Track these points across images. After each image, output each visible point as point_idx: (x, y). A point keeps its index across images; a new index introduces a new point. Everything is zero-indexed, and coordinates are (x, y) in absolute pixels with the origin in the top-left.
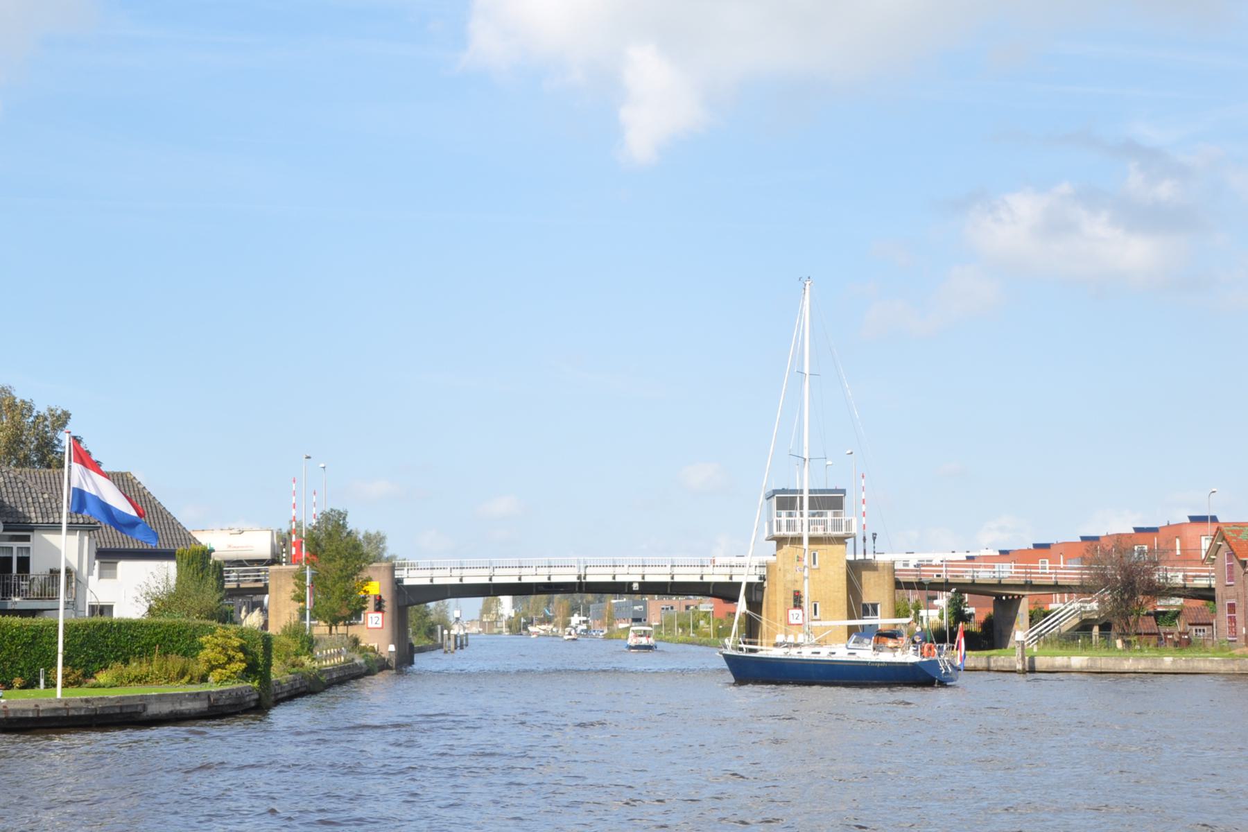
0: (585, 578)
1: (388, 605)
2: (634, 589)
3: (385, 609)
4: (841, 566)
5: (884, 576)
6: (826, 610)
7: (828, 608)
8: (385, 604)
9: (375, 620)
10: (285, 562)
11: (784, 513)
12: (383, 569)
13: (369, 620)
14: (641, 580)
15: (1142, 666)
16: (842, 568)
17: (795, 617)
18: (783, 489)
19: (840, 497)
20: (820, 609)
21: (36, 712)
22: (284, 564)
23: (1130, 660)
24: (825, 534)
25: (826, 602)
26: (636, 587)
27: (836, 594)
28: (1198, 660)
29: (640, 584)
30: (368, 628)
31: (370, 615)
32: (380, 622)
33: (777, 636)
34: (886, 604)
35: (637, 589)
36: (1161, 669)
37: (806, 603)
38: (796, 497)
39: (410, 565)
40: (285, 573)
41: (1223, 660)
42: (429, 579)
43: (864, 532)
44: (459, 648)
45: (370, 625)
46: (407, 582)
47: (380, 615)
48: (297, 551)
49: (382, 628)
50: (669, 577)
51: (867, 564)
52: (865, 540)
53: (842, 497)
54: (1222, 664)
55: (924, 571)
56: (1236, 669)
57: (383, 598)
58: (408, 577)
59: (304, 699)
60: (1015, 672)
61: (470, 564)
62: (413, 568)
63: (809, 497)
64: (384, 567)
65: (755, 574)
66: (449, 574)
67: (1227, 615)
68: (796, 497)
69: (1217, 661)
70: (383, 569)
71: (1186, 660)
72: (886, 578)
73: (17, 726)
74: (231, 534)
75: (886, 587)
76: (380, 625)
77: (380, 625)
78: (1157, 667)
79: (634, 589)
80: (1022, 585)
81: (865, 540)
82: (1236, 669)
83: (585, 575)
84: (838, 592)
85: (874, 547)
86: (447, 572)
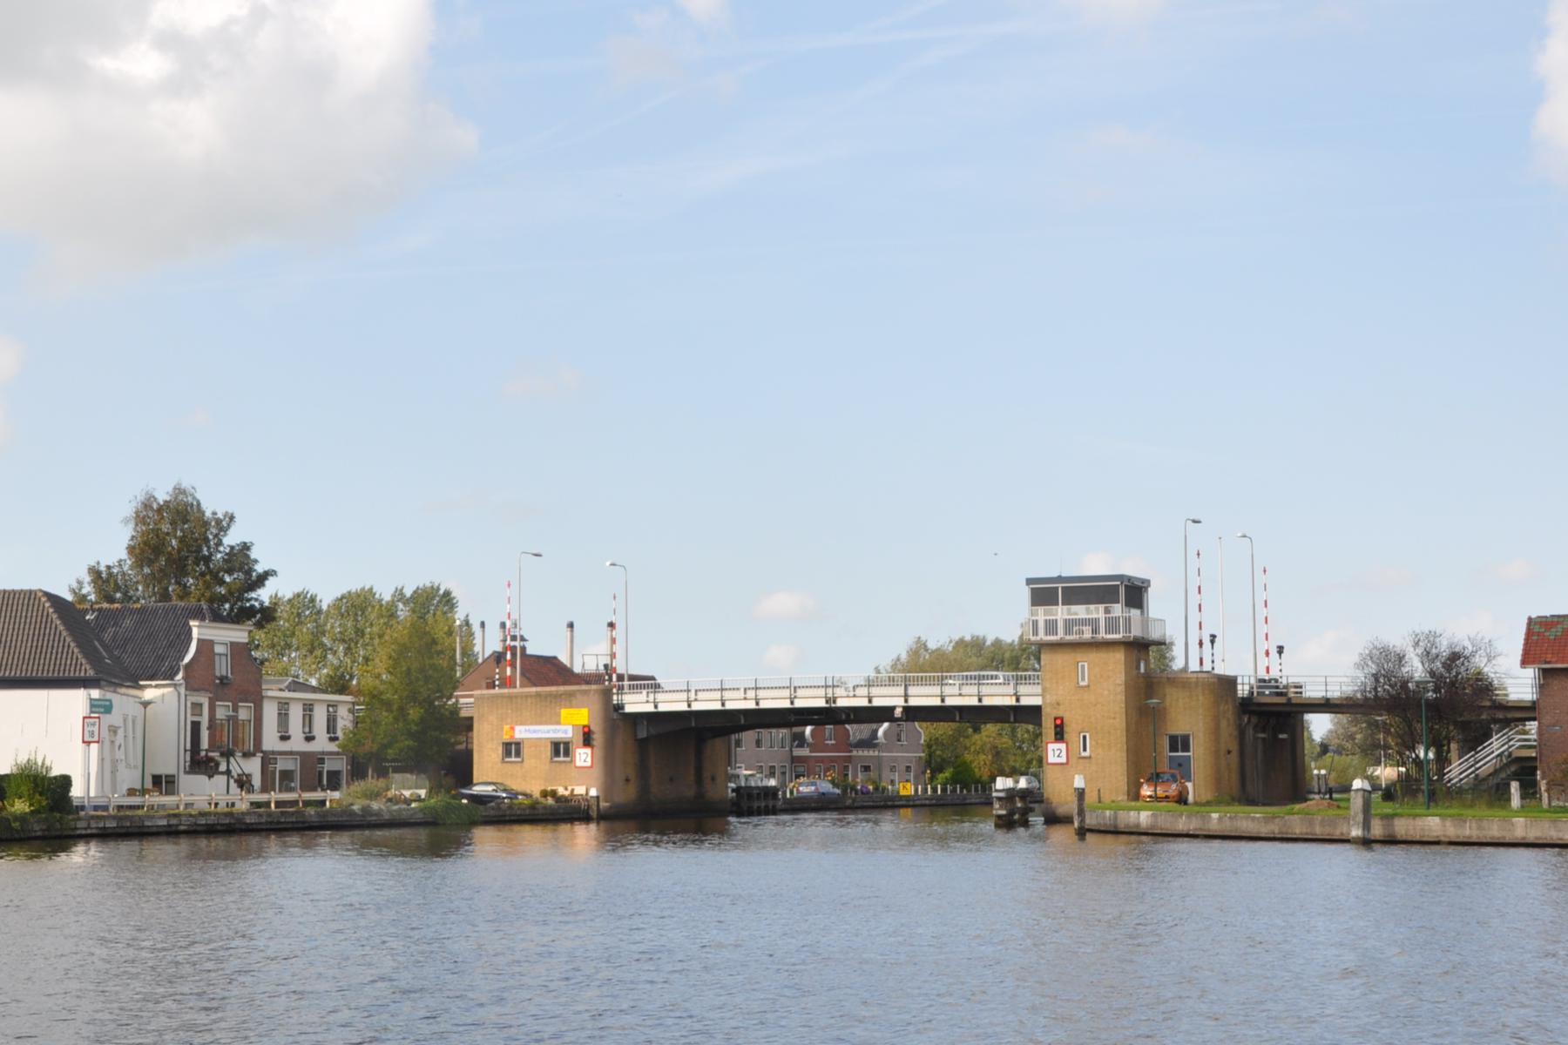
0: (834, 702)
1: (598, 738)
2: (896, 716)
3: (595, 743)
5: (1197, 696)
7: (1099, 741)
8: (595, 736)
9: (583, 757)
10: (498, 686)
11: (1041, 609)
12: (592, 692)
14: (903, 704)
15: (1451, 831)
16: (1119, 685)
17: (1057, 753)
18: (1060, 577)
19: (1054, 588)
20: (1090, 743)
22: (497, 688)
23: (1184, 818)
24: (1093, 638)
25: (1097, 733)
26: (898, 712)
27: (1112, 721)
28: (1241, 818)
29: (904, 708)
30: (576, 767)
32: (589, 759)
34: (1201, 735)
35: (900, 716)
36: (1209, 830)
38: (1057, 588)
39: (896, 679)
40: (488, 698)
41: (1264, 817)
43: (1201, 634)
44: (770, 797)
46: (629, 709)
47: (588, 750)
48: (512, 672)
49: (592, 767)
51: (1174, 678)
52: (1201, 644)
53: (1118, 585)
54: (1263, 824)
56: (1276, 831)
57: (592, 728)
58: (696, 700)
59: (232, 839)
60: (1347, 841)
62: (1023, 682)
64: (594, 690)
65: (647, 702)
66: (957, 692)
67: (1190, 754)
68: (1057, 588)
69: (1258, 818)
70: (592, 692)
71: (1230, 818)
72: (1201, 698)
75: (1201, 711)
76: (589, 764)
77: (589, 764)
78: (1206, 827)
79: (896, 716)
81: (1201, 644)
82: (1276, 831)
84: (1114, 718)
85: (1213, 655)
86: (741, 694)
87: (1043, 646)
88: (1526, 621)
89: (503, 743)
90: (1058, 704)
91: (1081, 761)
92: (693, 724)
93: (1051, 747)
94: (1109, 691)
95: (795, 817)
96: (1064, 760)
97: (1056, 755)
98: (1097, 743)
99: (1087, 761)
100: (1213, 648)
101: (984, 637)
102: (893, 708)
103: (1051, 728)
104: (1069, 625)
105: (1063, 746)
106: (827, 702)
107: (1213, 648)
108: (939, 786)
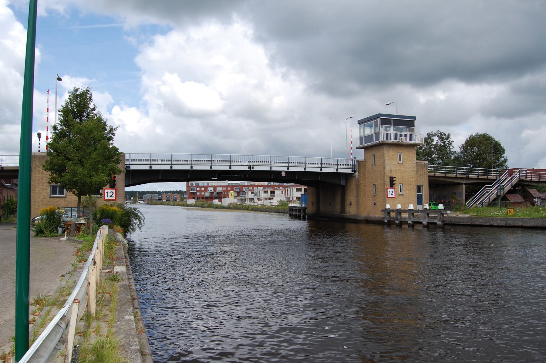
0: (253, 168)
4: (414, 162)
6: (406, 189)
7: (407, 188)
9: (110, 194)
13: (106, 194)
17: (391, 193)
21: (207, 184)
27: (411, 179)
31: (106, 191)
33: (134, 109)
37: (397, 186)
42: (320, 168)
45: (106, 198)
46: (133, 168)
50: (303, 168)
55: (444, 170)
61: (224, 158)
63: (414, 127)
67: (422, 193)
73: (226, 183)
74: (419, 189)
80: (537, 181)
83: (253, 166)
84: (412, 178)
87: (382, 145)
88: (37, 135)
89: (297, 191)
90: (391, 171)
91: (400, 196)
92: (296, 178)
93: (389, 190)
94: (410, 166)
95: (481, 224)
96: (114, 198)
97: (391, 194)
98: (406, 189)
99: (402, 196)
100: (39, 140)
101: (112, 130)
102: (280, 172)
103: (388, 182)
104: (396, 137)
105: (114, 191)
106: (249, 168)
107: (39, 140)
108: (89, 212)
